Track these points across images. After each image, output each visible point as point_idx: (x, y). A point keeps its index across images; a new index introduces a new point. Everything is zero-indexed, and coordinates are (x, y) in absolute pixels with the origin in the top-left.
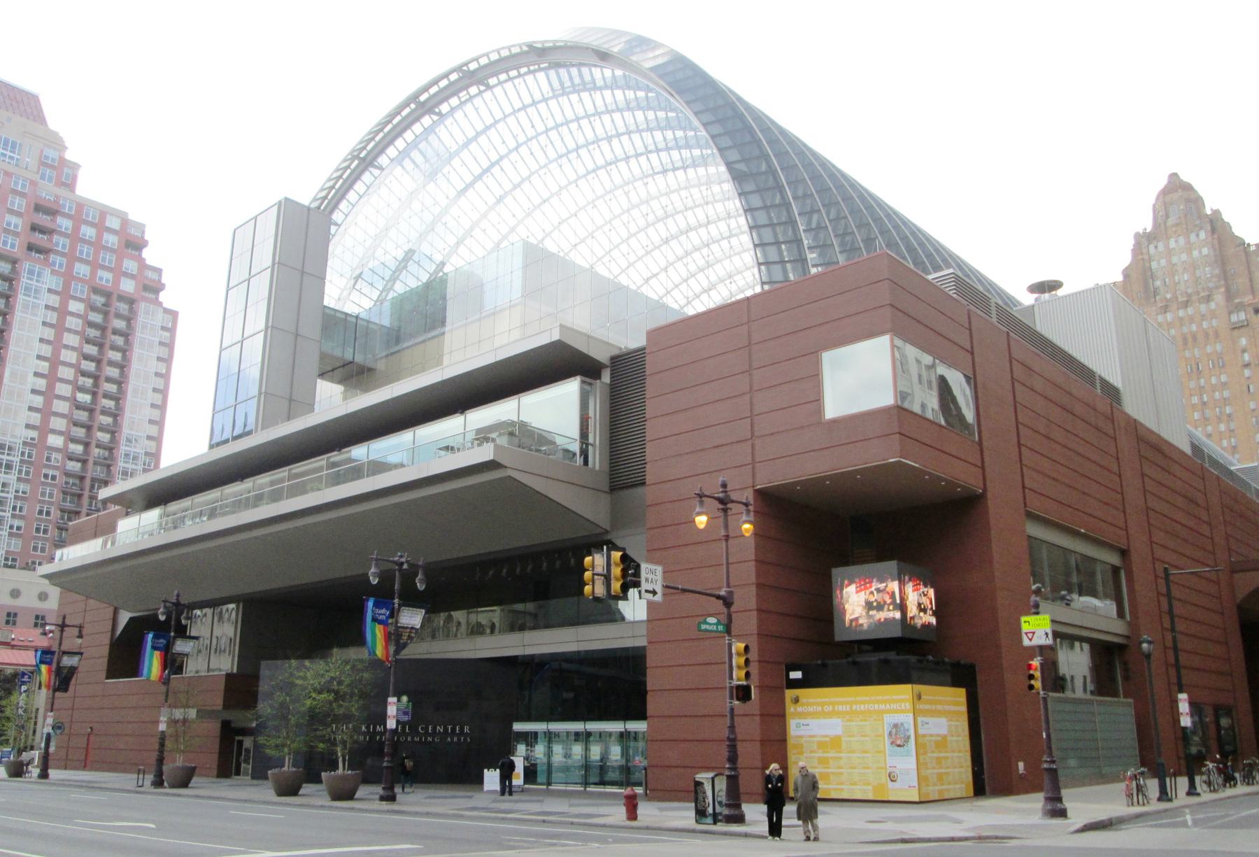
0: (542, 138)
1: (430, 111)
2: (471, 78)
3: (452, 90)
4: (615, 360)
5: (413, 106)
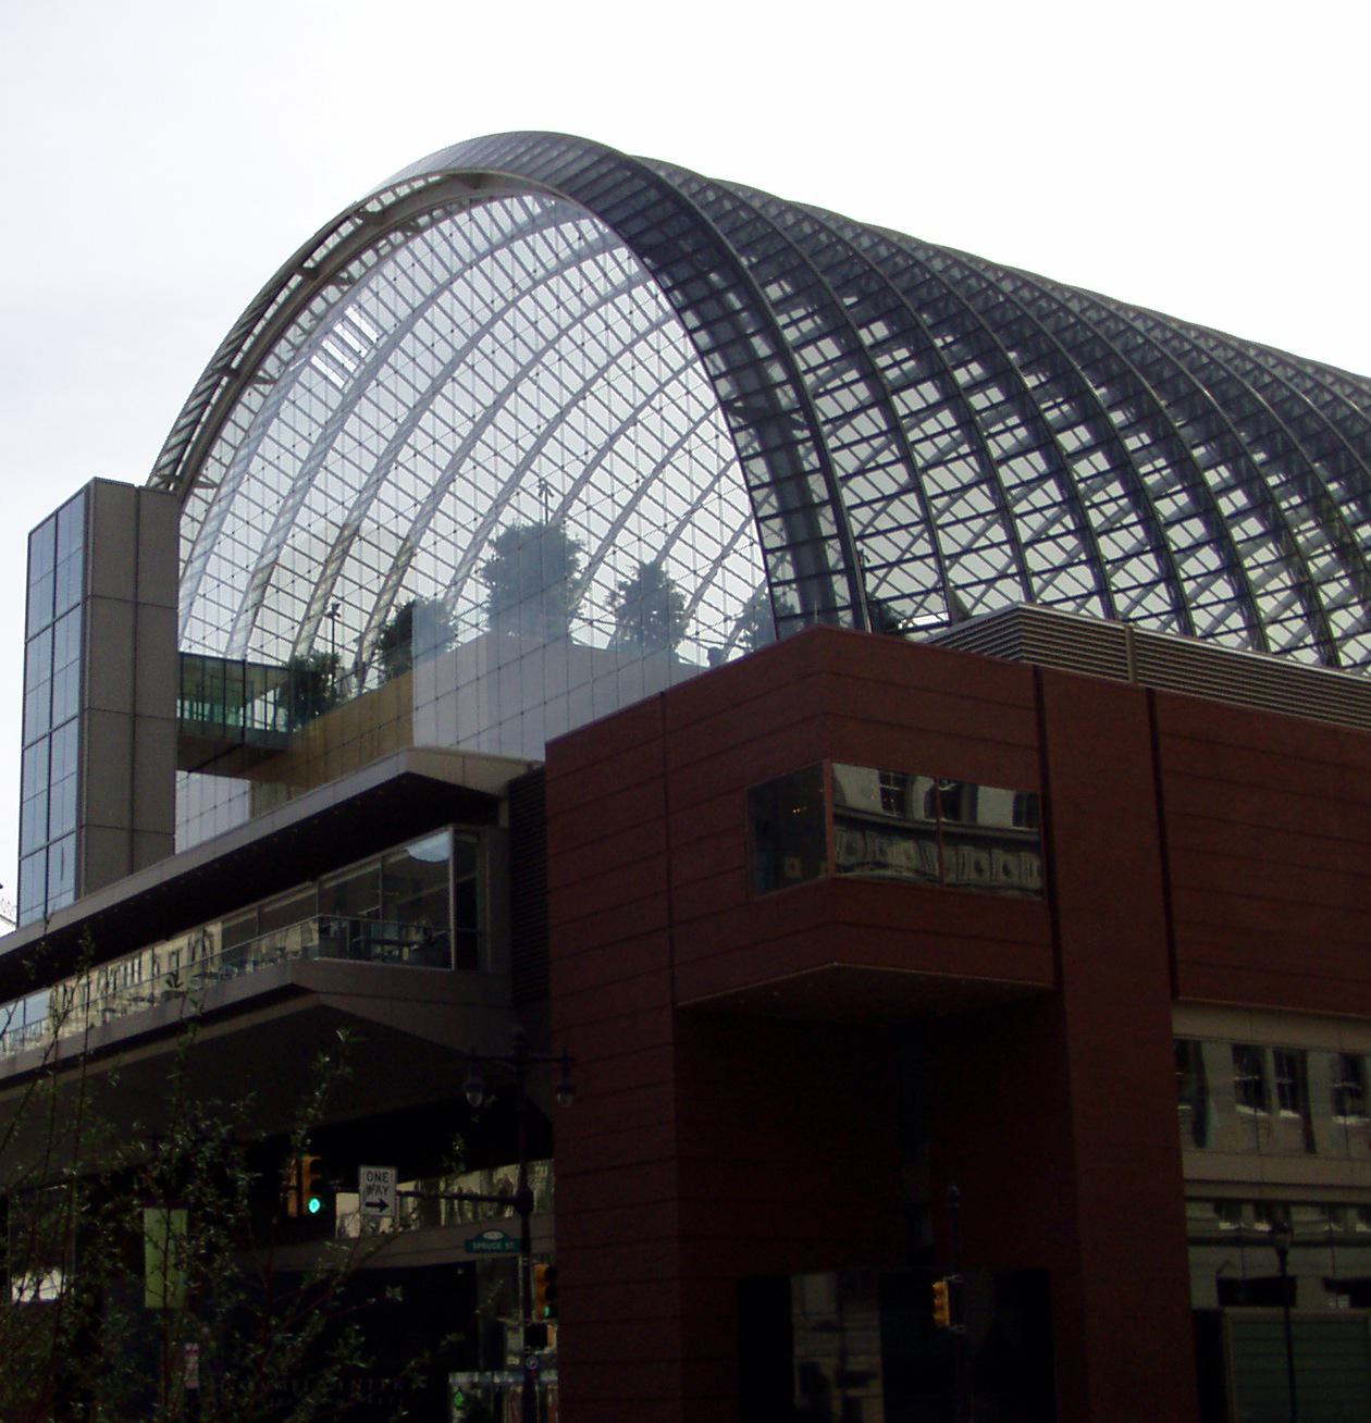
0: (565, 320)
1: (333, 279)
2: (376, 226)
3: (351, 250)
4: (515, 787)
5: (225, 381)
